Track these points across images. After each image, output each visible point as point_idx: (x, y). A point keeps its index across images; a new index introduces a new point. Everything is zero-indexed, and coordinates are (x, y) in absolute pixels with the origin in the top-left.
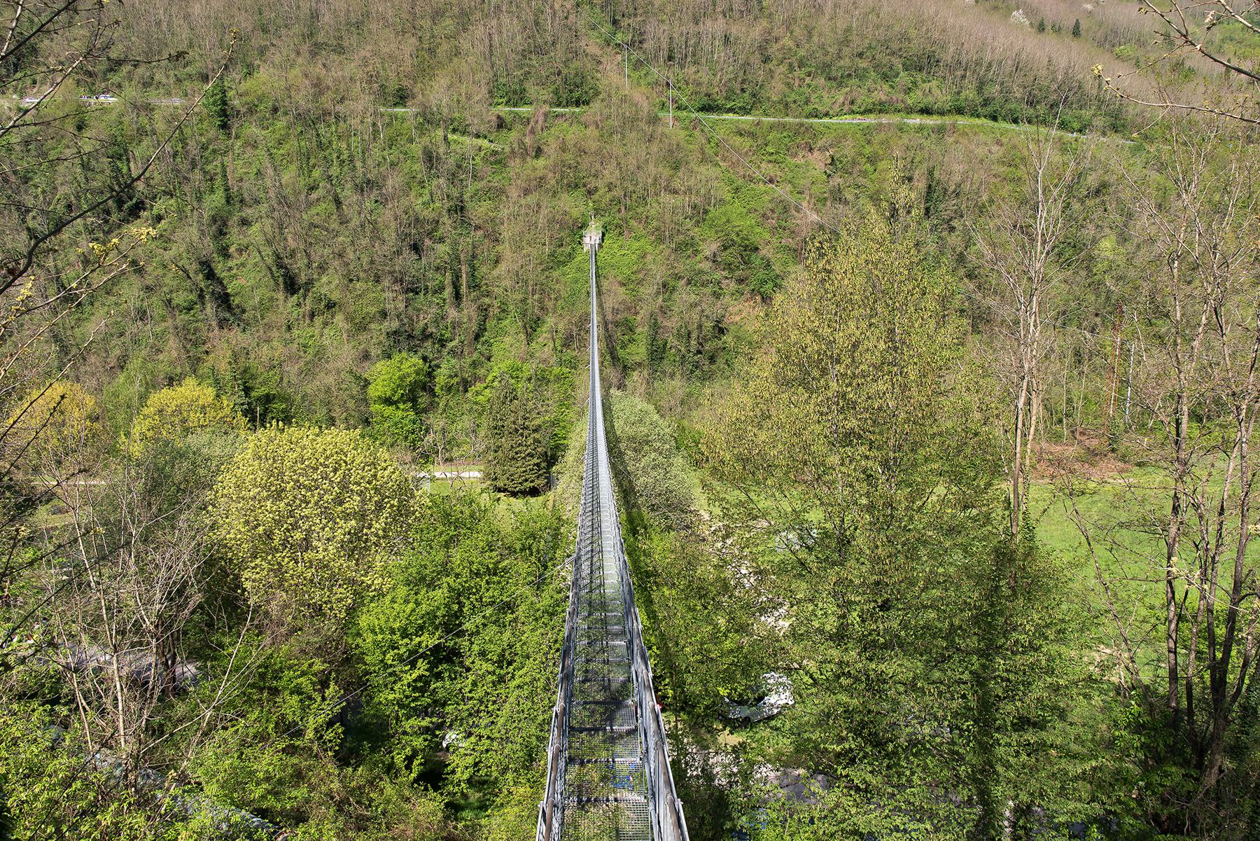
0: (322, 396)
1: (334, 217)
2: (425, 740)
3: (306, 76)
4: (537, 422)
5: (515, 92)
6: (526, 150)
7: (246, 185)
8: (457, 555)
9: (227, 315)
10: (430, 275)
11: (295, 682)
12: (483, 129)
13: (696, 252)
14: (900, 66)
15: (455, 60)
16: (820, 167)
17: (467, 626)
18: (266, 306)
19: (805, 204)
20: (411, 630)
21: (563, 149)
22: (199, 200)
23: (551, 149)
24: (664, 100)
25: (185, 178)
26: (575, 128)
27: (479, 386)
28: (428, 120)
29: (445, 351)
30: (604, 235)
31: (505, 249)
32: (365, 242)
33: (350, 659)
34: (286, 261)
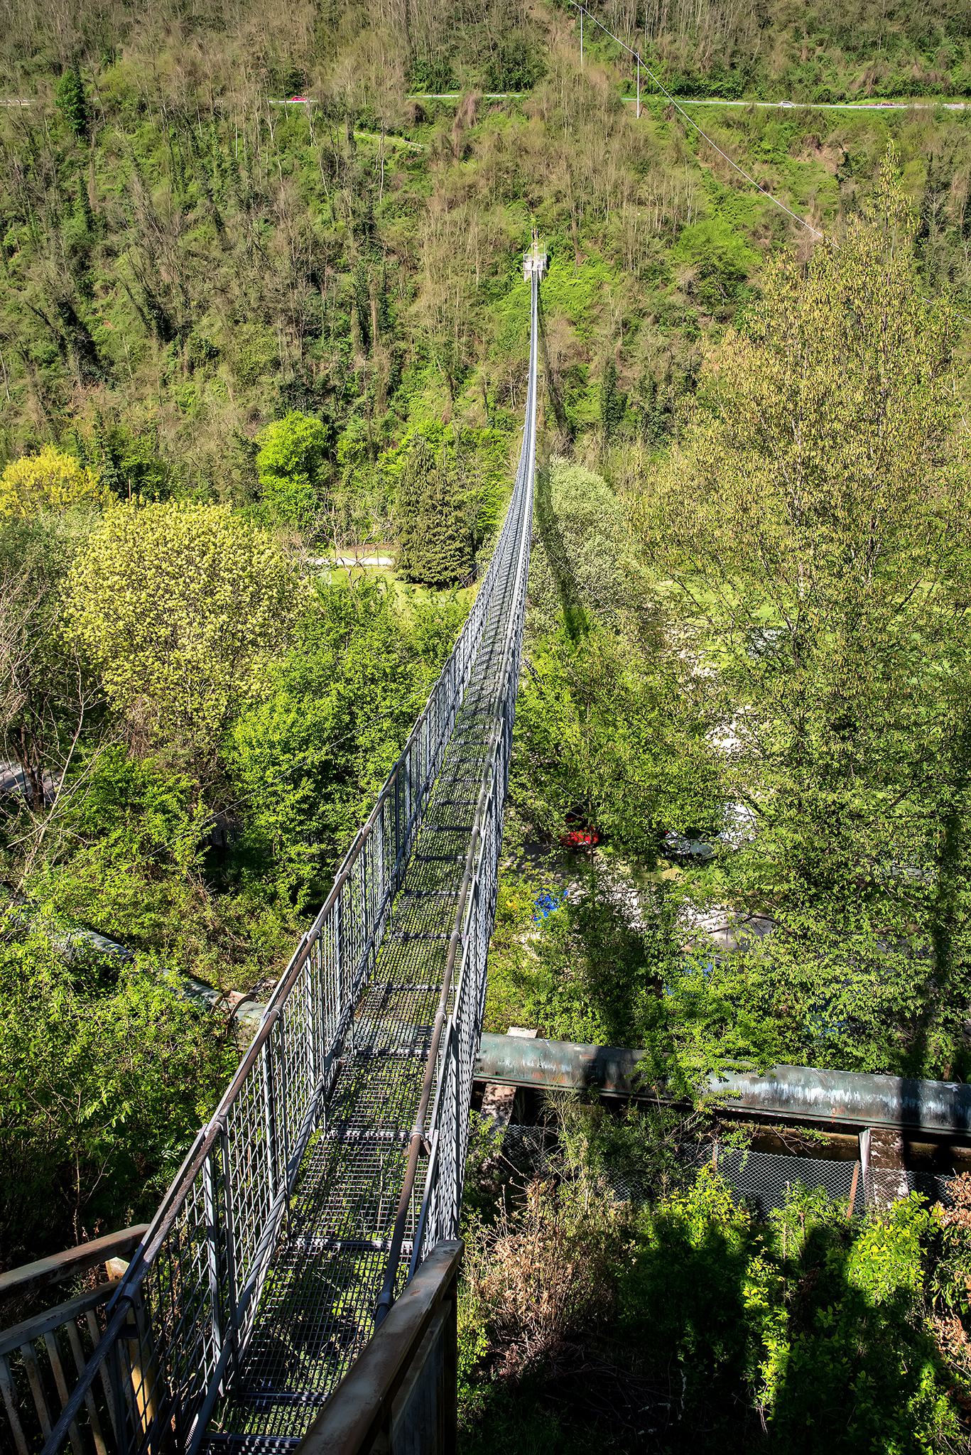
0: (202, 465)
1: (215, 242)
2: (314, 869)
3: (179, 61)
4: (458, 497)
5: (438, 74)
6: (452, 150)
7: (109, 205)
8: (348, 657)
9: (93, 368)
10: (331, 313)
11: (160, 799)
12: (397, 123)
13: (667, 281)
14: (942, 30)
15: (363, 33)
16: (831, 168)
17: (361, 741)
18: (137, 357)
19: (808, 218)
20: (293, 745)
21: (499, 148)
22: (56, 225)
23: (484, 149)
24: (630, 80)
25: (39, 199)
26: (514, 119)
27: (391, 452)
28: (329, 113)
29: (351, 410)
30: (549, 259)
31: (425, 279)
32: (252, 273)
33: (227, 777)
34: (159, 299)
